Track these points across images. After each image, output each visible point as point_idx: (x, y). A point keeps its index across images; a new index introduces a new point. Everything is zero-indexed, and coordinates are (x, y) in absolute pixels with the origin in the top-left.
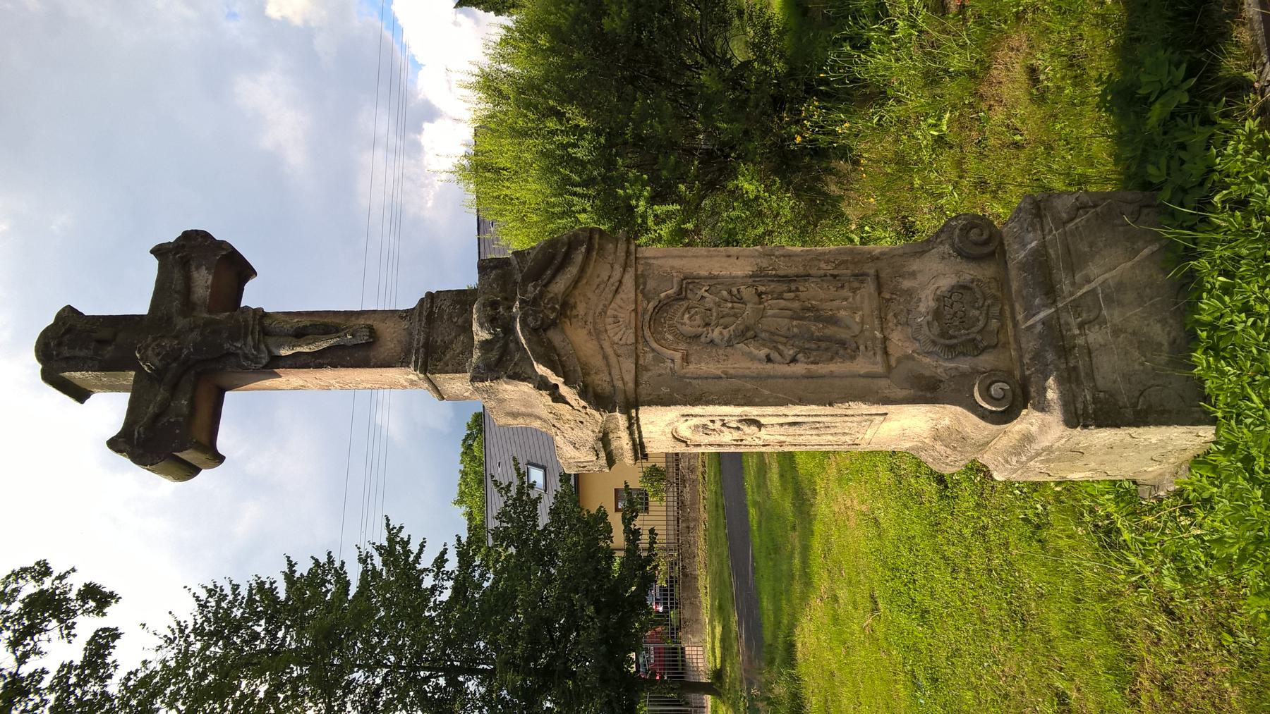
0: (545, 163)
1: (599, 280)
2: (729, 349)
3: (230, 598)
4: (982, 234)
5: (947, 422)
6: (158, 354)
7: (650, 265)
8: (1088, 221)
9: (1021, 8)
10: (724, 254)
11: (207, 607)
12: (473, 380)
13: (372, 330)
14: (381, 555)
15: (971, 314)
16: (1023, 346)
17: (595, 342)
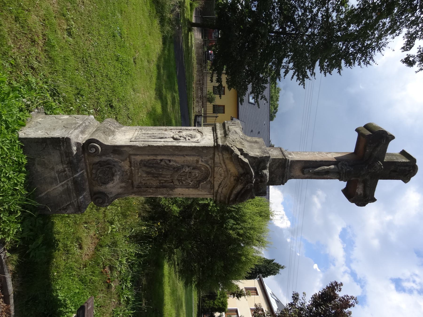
0: (244, 218)
3: (361, 61)
4: (98, 201)
5: (110, 138)
6: (376, 167)
7: (209, 192)
8: (63, 205)
9: (85, 269)
11: (370, 57)
12: (269, 157)
13: (303, 172)
14: (307, 75)
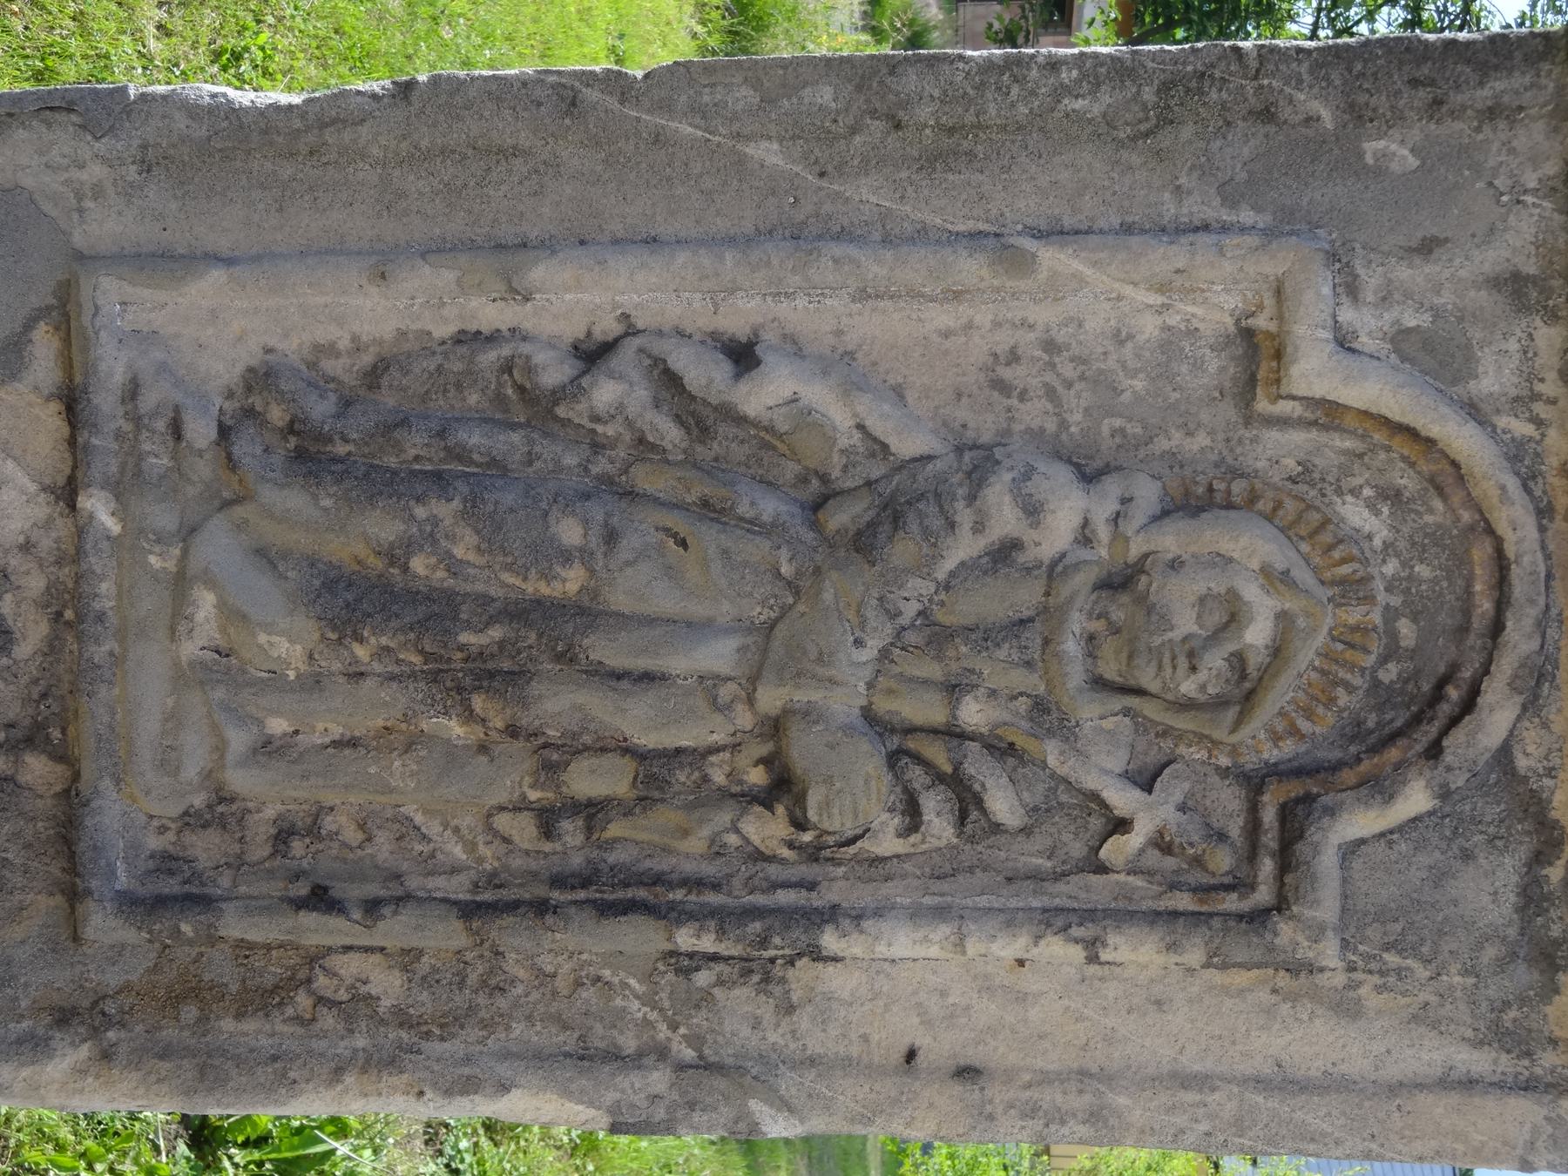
2: (985, 427)
7: (1500, 1036)
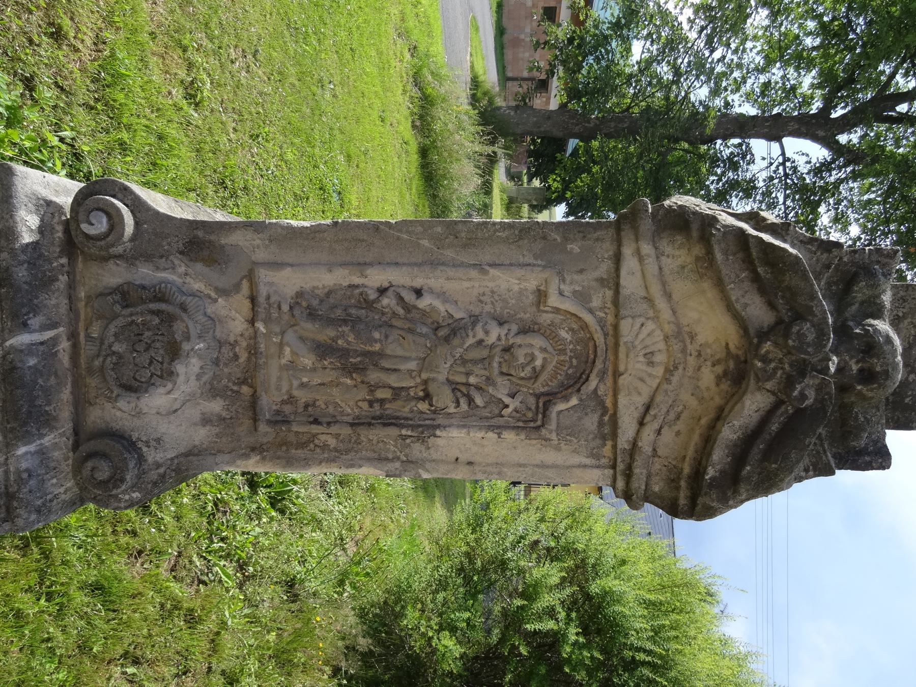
1: (676, 428)
2: (477, 311)
4: (93, 469)
7: (592, 455)
10: (477, 468)
15: (124, 346)
16: (67, 301)
17: (684, 321)
